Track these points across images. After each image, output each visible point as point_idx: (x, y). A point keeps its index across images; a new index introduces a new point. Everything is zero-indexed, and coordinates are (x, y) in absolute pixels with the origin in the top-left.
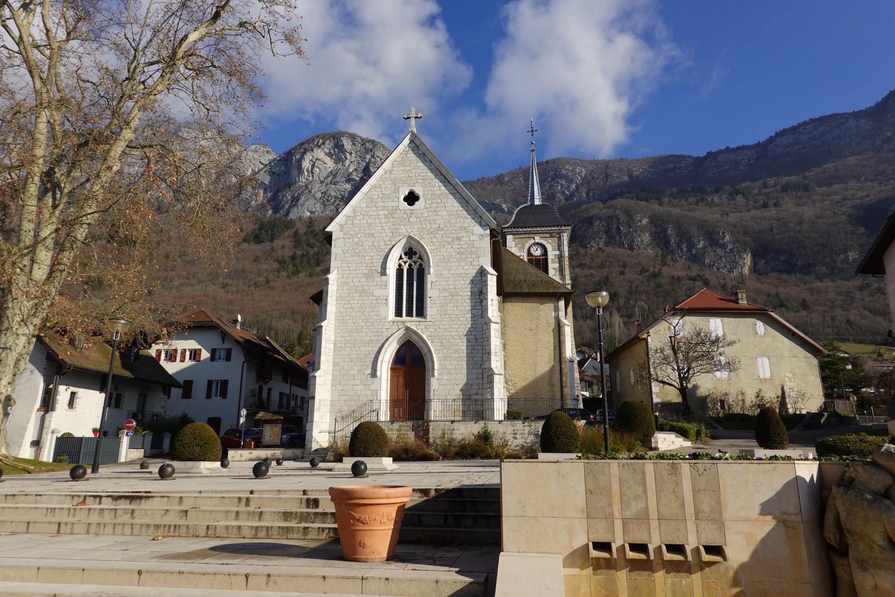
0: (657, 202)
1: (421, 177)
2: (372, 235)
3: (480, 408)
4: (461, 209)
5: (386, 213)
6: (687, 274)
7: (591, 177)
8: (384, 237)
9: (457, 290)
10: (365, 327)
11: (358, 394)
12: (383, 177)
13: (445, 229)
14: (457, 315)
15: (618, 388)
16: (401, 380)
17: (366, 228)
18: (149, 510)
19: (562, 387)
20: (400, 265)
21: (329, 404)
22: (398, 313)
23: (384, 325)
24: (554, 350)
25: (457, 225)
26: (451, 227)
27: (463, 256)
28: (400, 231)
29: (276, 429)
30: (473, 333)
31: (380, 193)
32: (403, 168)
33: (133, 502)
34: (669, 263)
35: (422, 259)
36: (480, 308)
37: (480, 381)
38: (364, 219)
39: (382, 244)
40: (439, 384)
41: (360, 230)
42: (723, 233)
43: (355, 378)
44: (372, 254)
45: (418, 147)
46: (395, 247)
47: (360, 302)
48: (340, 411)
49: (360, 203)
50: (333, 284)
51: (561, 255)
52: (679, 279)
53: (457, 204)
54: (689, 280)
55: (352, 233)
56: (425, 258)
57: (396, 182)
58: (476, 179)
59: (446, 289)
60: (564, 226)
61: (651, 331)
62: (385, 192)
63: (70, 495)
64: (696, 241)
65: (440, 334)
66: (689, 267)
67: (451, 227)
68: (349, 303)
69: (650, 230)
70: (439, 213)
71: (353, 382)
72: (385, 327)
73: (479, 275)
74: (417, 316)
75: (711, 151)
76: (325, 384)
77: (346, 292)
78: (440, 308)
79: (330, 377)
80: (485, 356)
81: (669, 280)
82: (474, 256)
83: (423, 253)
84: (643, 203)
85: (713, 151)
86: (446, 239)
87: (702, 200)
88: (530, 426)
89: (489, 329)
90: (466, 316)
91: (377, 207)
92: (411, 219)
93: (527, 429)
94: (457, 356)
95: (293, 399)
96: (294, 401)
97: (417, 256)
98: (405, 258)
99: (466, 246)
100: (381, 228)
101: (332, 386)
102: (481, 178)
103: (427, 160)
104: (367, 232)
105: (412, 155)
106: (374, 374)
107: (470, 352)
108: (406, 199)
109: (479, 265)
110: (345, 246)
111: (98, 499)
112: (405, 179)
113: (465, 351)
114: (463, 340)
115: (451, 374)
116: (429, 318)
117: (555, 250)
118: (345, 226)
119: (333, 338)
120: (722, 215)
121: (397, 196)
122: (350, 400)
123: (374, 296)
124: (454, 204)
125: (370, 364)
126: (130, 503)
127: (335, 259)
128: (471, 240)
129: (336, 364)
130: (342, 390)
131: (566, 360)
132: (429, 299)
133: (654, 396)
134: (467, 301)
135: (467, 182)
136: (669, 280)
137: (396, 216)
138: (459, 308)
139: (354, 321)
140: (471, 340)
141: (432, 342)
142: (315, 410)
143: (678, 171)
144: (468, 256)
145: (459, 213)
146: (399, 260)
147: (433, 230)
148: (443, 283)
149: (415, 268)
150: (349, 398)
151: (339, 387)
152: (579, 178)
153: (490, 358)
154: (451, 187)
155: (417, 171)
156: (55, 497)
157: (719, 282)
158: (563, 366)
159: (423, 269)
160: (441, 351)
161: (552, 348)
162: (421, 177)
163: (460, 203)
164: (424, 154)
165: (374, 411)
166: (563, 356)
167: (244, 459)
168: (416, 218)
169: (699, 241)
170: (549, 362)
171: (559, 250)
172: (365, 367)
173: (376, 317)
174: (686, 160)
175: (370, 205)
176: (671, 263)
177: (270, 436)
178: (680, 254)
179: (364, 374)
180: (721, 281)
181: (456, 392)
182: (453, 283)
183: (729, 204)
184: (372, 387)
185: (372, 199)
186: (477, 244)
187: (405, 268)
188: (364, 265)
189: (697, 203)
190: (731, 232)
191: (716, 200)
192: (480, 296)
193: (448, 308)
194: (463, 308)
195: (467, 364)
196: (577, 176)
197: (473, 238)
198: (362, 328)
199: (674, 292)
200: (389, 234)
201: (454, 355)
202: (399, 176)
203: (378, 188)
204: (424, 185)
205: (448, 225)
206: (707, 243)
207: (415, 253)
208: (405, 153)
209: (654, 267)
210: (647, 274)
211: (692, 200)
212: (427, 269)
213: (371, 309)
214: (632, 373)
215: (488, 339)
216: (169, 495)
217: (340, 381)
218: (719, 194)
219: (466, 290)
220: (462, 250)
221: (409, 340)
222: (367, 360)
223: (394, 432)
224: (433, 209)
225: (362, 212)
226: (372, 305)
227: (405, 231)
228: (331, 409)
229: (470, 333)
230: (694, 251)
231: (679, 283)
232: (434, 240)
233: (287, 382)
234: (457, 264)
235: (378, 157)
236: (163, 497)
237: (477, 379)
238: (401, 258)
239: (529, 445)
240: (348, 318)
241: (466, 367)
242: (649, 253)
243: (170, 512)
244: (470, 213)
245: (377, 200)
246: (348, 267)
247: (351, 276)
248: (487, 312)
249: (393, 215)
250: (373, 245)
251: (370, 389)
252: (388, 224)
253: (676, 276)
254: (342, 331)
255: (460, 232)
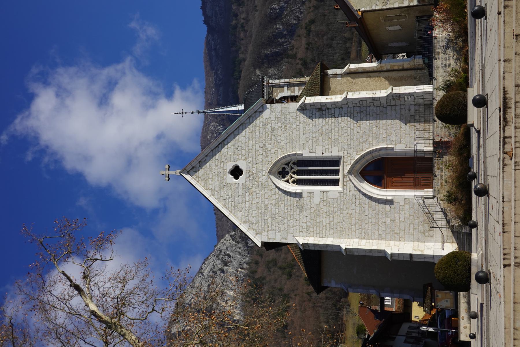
0: (242, 63)
1: (219, 164)
2: (266, 206)
3: (422, 106)
4: (247, 129)
5: (247, 194)
6: (305, 37)
7: (218, 118)
8: (269, 196)
9: (317, 130)
10: (347, 211)
11: (408, 217)
12: (216, 198)
13: (264, 142)
14: (339, 130)
15: (404, 44)
16: (395, 179)
17: (260, 211)
18: (515, 71)
19: (403, 70)
20: (294, 182)
21: (418, 243)
22: (336, 182)
23: (346, 194)
24: (370, 77)
25: (261, 132)
26: (262, 138)
27: (288, 126)
28: (264, 181)
29: (440, 296)
30: (355, 115)
31: (230, 200)
32: (210, 180)
33: (509, 106)
34: (294, 52)
35: (289, 163)
36: (333, 110)
37: (398, 108)
38: (252, 214)
39: (274, 197)
40: (400, 143)
41: (261, 217)
42: (271, 9)
43: (394, 219)
44: (283, 206)
45: (193, 168)
46: (277, 184)
47: (325, 216)
48: (424, 233)
49: (237, 217)
50: (308, 240)
51: (287, 85)
52: (308, 44)
53: (244, 133)
54: (309, 35)
55: (263, 224)
56: (288, 159)
57: (222, 185)
58: (215, 216)
59: (316, 140)
60: (263, 82)
61: (356, 8)
62: (230, 194)
63: (503, 167)
64: (277, 31)
65: (355, 144)
66: (299, 36)
67: (262, 138)
68: (326, 226)
69: (266, 68)
70: (250, 148)
71: (397, 221)
72: (348, 193)
73: (305, 112)
74: (338, 165)
75: (203, 21)
76: (399, 246)
77: (315, 229)
78: (332, 144)
79: (392, 243)
80: (376, 103)
81: (309, 52)
82: (288, 117)
83: (283, 161)
84: (243, 74)
85: (203, 19)
86: (273, 141)
87: (242, 27)
88: (439, 53)
89: (353, 100)
90: (340, 121)
91: (242, 202)
92: (254, 172)
93: (441, 56)
94: (375, 128)
95: (411, 334)
96: (412, 334)
97: (286, 166)
98: (288, 177)
99: (279, 124)
100: (261, 198)
101: (400, 241)
102: (214, 212)
103: (205, 159)
104: (263, 210)
105: (200, 173)
106: (390, 202)
107: (371, 118)
108: (237, 178)
109: (296, 112)
110: (275, 230)
111: (506, 140)
112: (220, 178)
113: (371, 122)
114: (361, 123)
115: (391, 133)
116: (341, 154)
117: (284, 90)
118: (257, 231)
119: (357, 240)
120: (256, 11)
121: (234, 184)
122: (413, 224)
123: (320, 204)
124: (243, 135)
125: (381, 206)
126: (510, 108)
127: (286, 239)
128: (274, 119)
129: (380, 237)
130: (405, 231)
131: (379, 66)
132: (324, 155)
133: (412, 4)
134: (327, 122)
135: (217, 224)
136: (309, 52)
137: (251, 185)
138: (333, 128)
139: (342, 220)
140: (362, 117)
141: (362, 150)
142: (422, 254)
143: (218, 47)
144: (288, 122)
145: (251, 130)
146: (289, 183)
147: (264, 153)
148: (311, 143)
149: (296, 168)
150: (412, 226)
151: (402, 233)
152: (219, 127)
153: (378, 97)
154: (229, 138)
155: (213, 167)
156: (505, 182)
157: (312, 12)
158: (385, 69)
159: (298, 161)
160: (371, 142)
161: (369, 79)
162: (219, 164)
163: (243, 130)
164: (200, 162)
165: (424, 202)
166: (376, 69)
167: (468, 325)
168: (253, 167)
169: (277, 29)
170: (381, 81)
171: (283, 87)
172: (384, 210)
173: (339, 201)
174: (210, 40)
175: (240, 209)
176: (295, 50)
177: (447, 301)
178: (288, 43)
179: (390, 211)
180: (311, 10)
181: (408, 129)
182: (311, 134)
183: (248, 5)
184: (402, 203)
185: (235, 206)
186: (278, 115)
187: (296, 177)
188: (292, 213)
189: (245, 31)
190: (271, 3)
191: (243, 16)
192: (323, 110)
193: (333, 138)
194: (333, 124)
195: (383, 120)
196: (217, 129)
197: (273, 118)
198: (348, 213)
199: (319, 47)
200: (267, 192)
201: (374, 131)
202: (217, 183)
203: (225, 202)
204: (225, 162)
205: (261, 139)
206: (279, 22)
207: (284, 169)
208: (198, 179)
209: (297, 64)
210: (303, 70)
211: (242, 35)
212: (298, 157)
213: (331, 206)
214: (391, 28)
215: (361, 100)
216: (502, 73)
217: (396, 233)
218: (239, 14)
219: (317, 122)
220: (283, 127)
221: (360, 173)
222: (377, 208)
223: (443, 174)
224: (247, 153)
225: (246, 215)
226: (327, 205)
227: (264, 177)
228: (422, 242)
229: (355, 118)
230: (285, 32)
231: (311, 43)
232: (273, 151)
233: (395, 338)
234: (294, 131)
235: (190, 301)
236: (504, 78)
237: (396, 110)
238: (287, 181)
239: (455, 54)
240: (338, 227)
241: (385, 121)
242: (285, 68)
243: (517, 51)
244: (251, 121)
245: (236, 202)
246: (293, 227)
247: (301, 224)
248: (338, 102)
249: (250, 188)
250: (275, 205)
251: (404, 206)
252: (258, 192)
253: (306, 46)
254: (350, 232)
255: (267, 129)
